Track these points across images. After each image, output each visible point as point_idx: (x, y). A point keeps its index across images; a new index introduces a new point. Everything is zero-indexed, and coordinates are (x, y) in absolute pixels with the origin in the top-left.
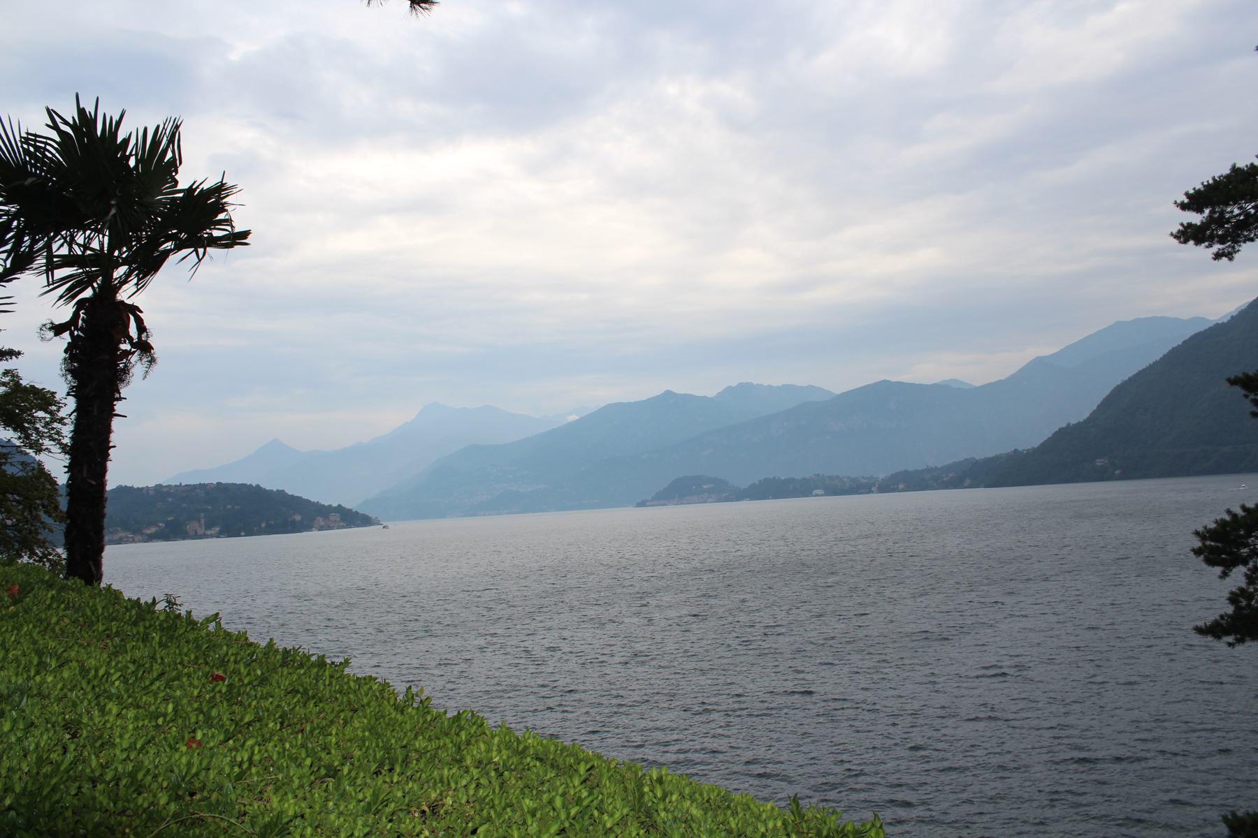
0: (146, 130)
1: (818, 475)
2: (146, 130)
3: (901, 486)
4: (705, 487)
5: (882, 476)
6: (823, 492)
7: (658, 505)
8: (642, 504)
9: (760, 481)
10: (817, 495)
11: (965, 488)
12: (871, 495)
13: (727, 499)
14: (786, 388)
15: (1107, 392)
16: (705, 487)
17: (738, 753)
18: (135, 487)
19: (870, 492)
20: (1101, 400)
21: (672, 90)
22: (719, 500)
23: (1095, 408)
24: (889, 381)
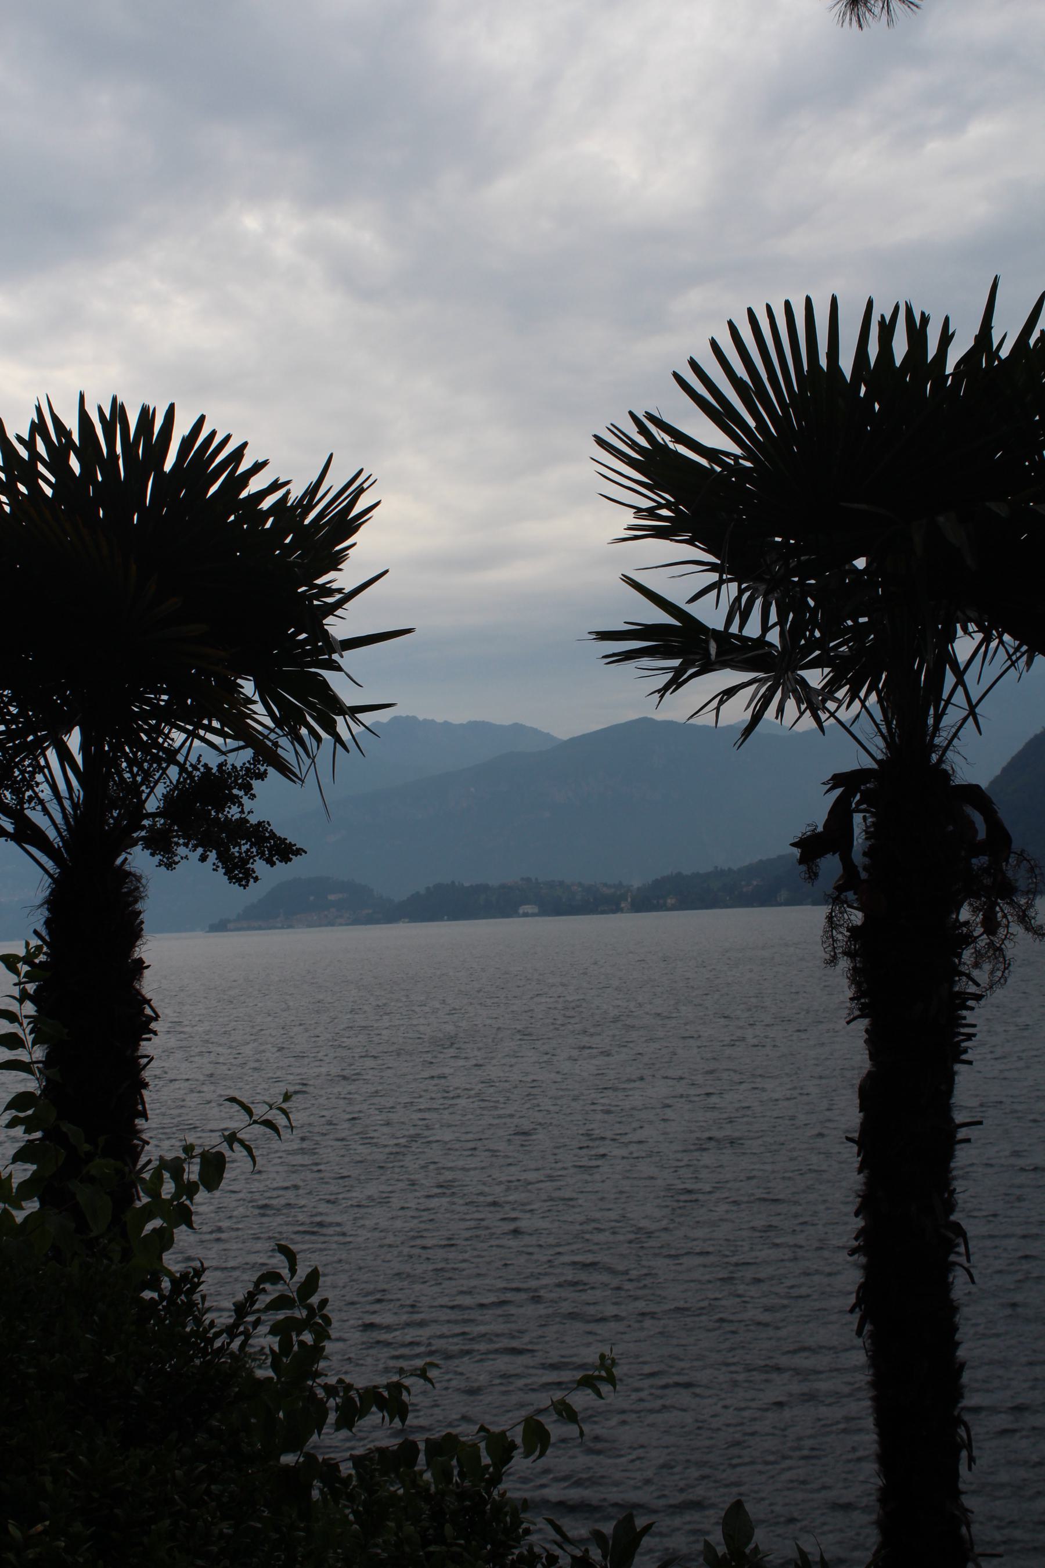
0: (228, 438)
1: (528, 880)
2: (228, 438)
3: (670, 901)
4: (332, 897)
5: (636, 883)
6: (536, 910)
7: (249, 928)
8: (220, 927)
9: (428, 888)
10: (526, 915)
11: (780, 905)
12: (619, 915)
13: (370, 920)
14: (477, 728)
15: (1017, 746)
16: (332, 897)
17: (602, 1151)
18: (421, 718)
19: (617, 909)
20: (1024, 744)
21: (251, 222)
22: (356, 922)
23: (997, 771)
24: (652, 719)
